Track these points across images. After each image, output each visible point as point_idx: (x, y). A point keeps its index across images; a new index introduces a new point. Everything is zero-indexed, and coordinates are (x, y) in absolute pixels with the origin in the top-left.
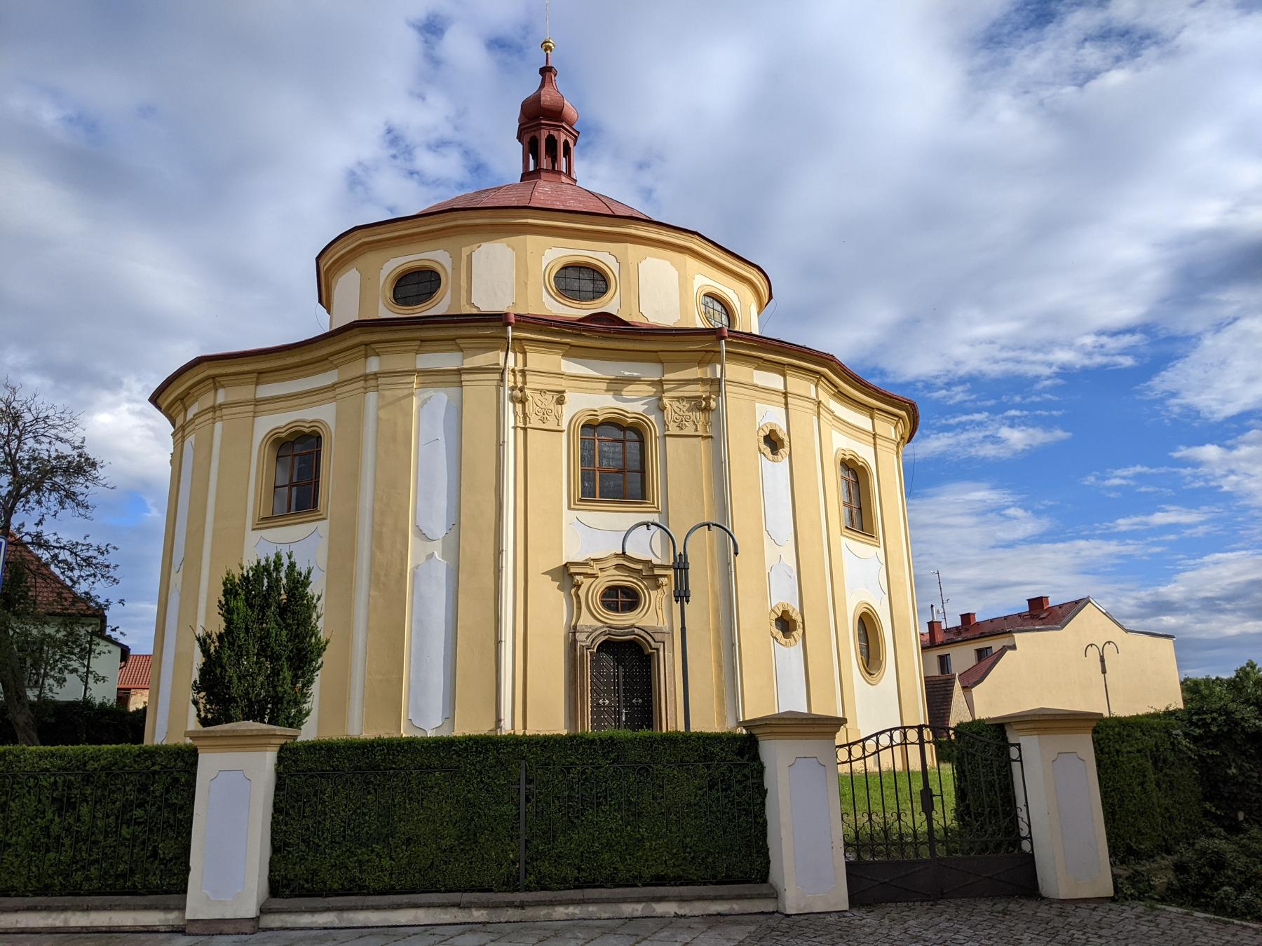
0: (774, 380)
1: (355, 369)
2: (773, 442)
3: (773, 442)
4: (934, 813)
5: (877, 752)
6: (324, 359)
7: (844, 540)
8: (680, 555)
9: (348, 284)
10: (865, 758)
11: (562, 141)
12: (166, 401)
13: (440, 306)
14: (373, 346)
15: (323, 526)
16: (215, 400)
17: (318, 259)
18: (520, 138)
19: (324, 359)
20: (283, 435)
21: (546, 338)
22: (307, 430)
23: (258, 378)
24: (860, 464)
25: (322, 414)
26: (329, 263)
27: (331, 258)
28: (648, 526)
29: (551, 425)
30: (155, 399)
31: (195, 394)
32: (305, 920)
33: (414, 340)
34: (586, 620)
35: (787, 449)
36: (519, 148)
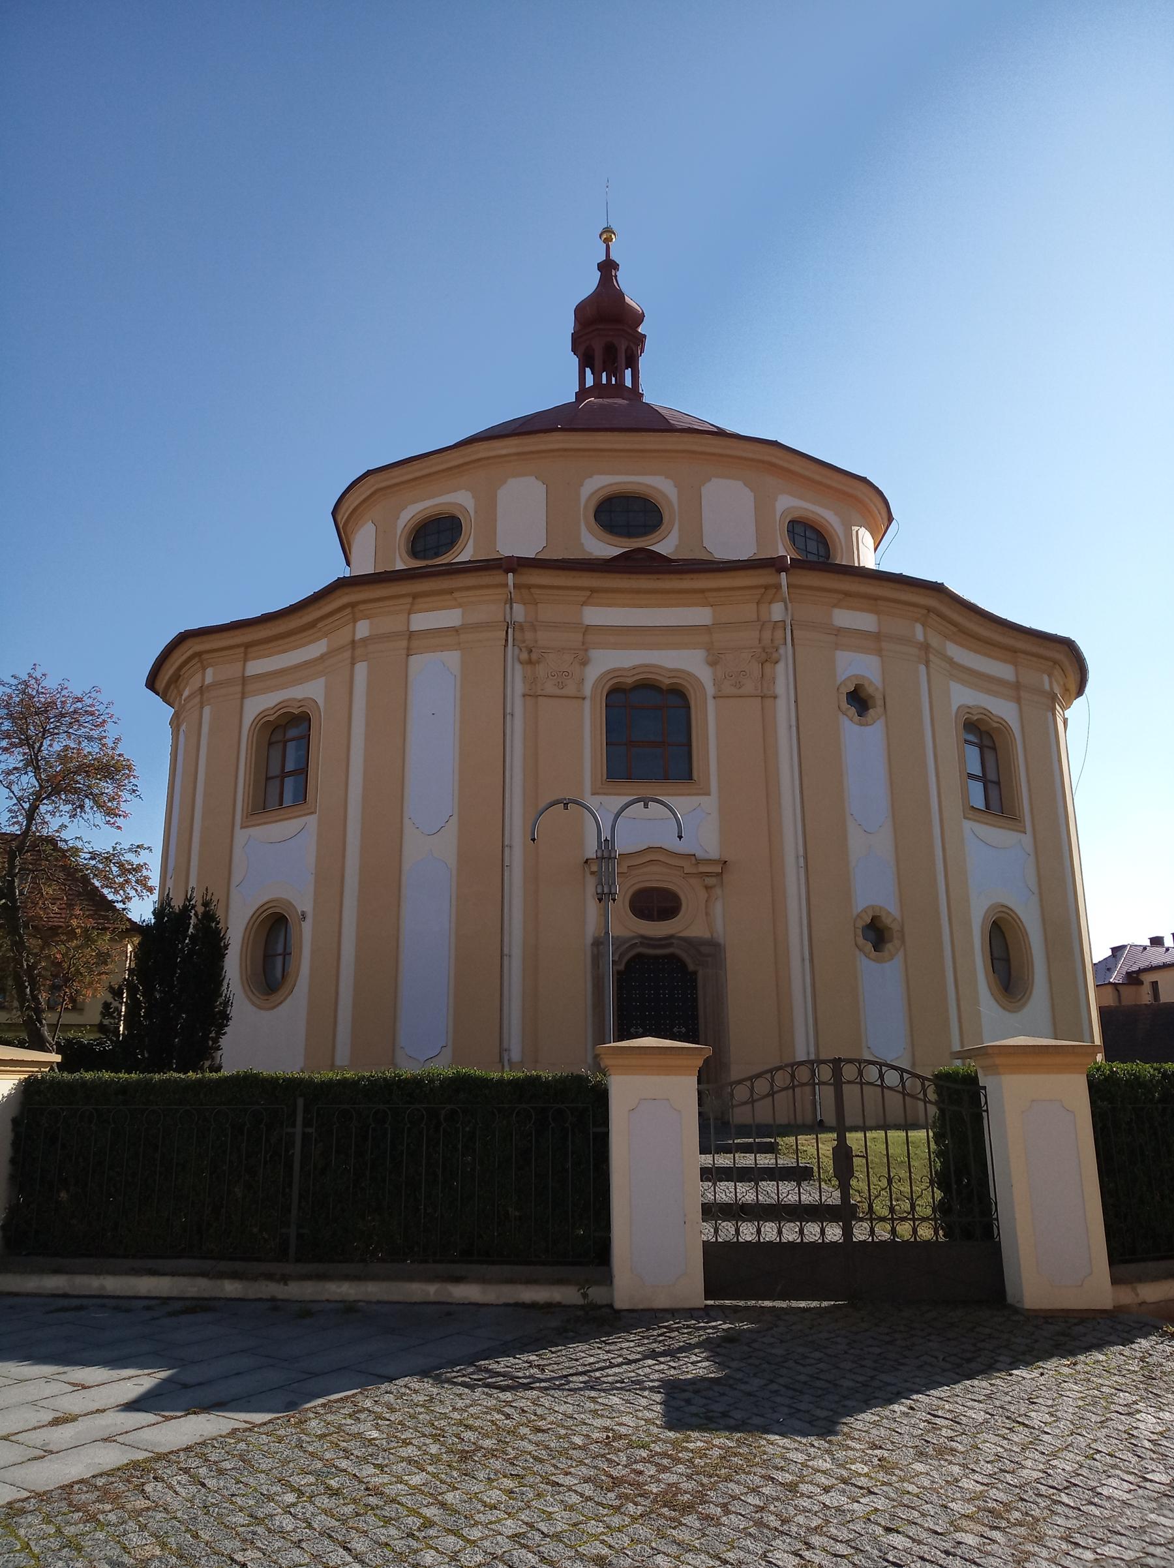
0: (864, 621)
1: (342, 636)
2: (859, 700)
3: (859, 700)
4: (853, 1182)
5: (772, 1094)
6: (312, 625)
7: (968, 825)
8: (606, 840)
9: (365, 537)
10: (753, 1102)
11: (623, 348)
12: (161, 684)
13: (466, 553)
14: (362, 607)
15: (312, 821)
16: (203, 680)
17: (334, 513)
18: (574, 350)
19: (312, 625)
20: (271, 718)
21: (420, 571)
22: (296, 712)
23: (246, 653)
24: (996, 725)
25: (312, 691)
26: (345, 517)
27: (345, 514)
28: (566, 805)
29: (570, 690)
30: (151, 684)
31: (186, 676)
32: (113, 1284)
33: (1047, 659)
34: (616, 930)
35: (880, 710)
36: (574, 361)
